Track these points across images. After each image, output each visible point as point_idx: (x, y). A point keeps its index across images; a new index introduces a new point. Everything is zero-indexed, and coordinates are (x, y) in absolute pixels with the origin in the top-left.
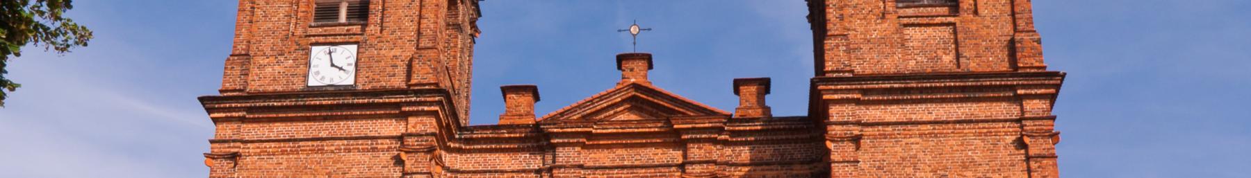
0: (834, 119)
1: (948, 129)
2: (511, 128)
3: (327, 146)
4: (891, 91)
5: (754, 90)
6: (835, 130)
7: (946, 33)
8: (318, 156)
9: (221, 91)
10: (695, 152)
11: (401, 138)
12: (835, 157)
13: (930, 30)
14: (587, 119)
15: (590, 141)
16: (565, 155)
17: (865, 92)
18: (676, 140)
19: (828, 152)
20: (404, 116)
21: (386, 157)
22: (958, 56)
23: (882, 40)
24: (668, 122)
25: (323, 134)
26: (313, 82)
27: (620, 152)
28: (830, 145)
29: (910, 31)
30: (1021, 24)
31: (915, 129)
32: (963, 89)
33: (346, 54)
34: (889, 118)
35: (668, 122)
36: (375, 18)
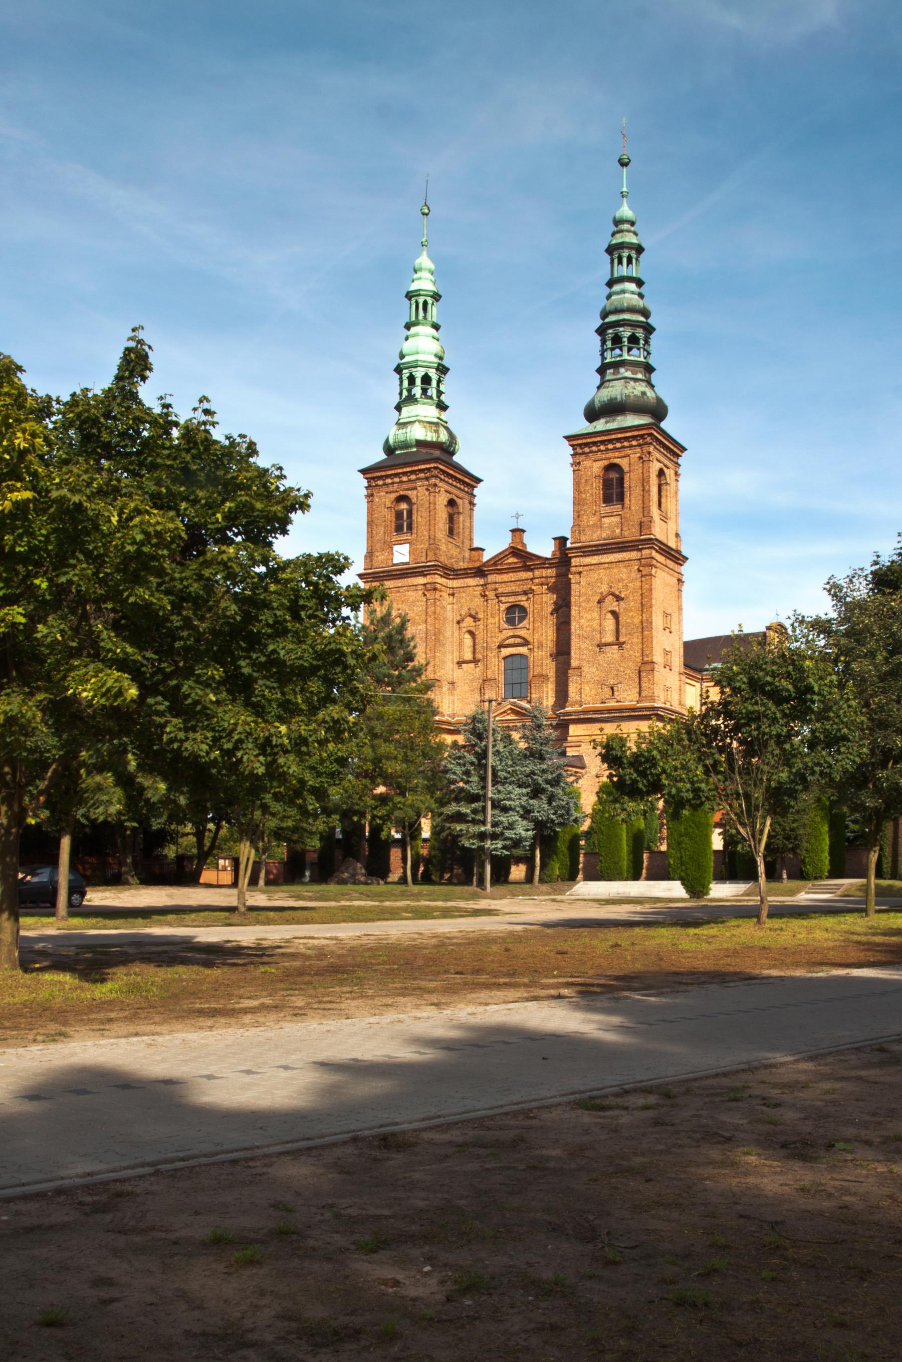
0: (573, 564)
1: (613, 565)
2: (470, 569)
3: (401, 590)
4: (592, 551)
5: (84, 753)
6: (573, 569)
7: (617, 519)
8: (398, 594)
9: (592, 414)
10: (537, 573)
11: (424, 585)
12: (573, 581)
13: (612, 518)
14: (495, 564)
15: (500, 572)
16: (491, 578)
17: (583, 552)
18: (528, 569)
19: (570, 579)
20: (425, 575)
21: (420, 592)
22: (622, 530)
23: (593, 525)
24: (525, 562)
25: (400, 585)
26: (395, 562)
27: (511, 574)
28: (570, 576)
29: (605, 520)
30: (646, 513)
31: (602, 566)
32: (619, 548)
33: (406, 548)
34: (594, 562)
35: (525, 562)
36: (414, 531)
